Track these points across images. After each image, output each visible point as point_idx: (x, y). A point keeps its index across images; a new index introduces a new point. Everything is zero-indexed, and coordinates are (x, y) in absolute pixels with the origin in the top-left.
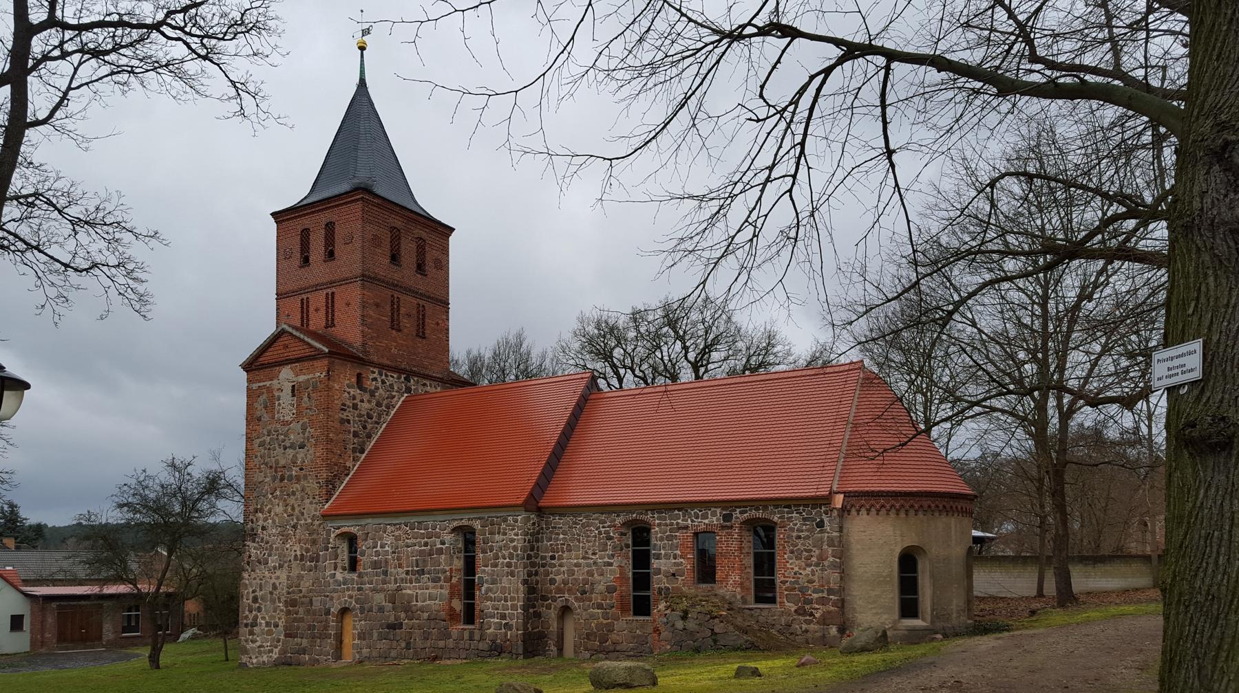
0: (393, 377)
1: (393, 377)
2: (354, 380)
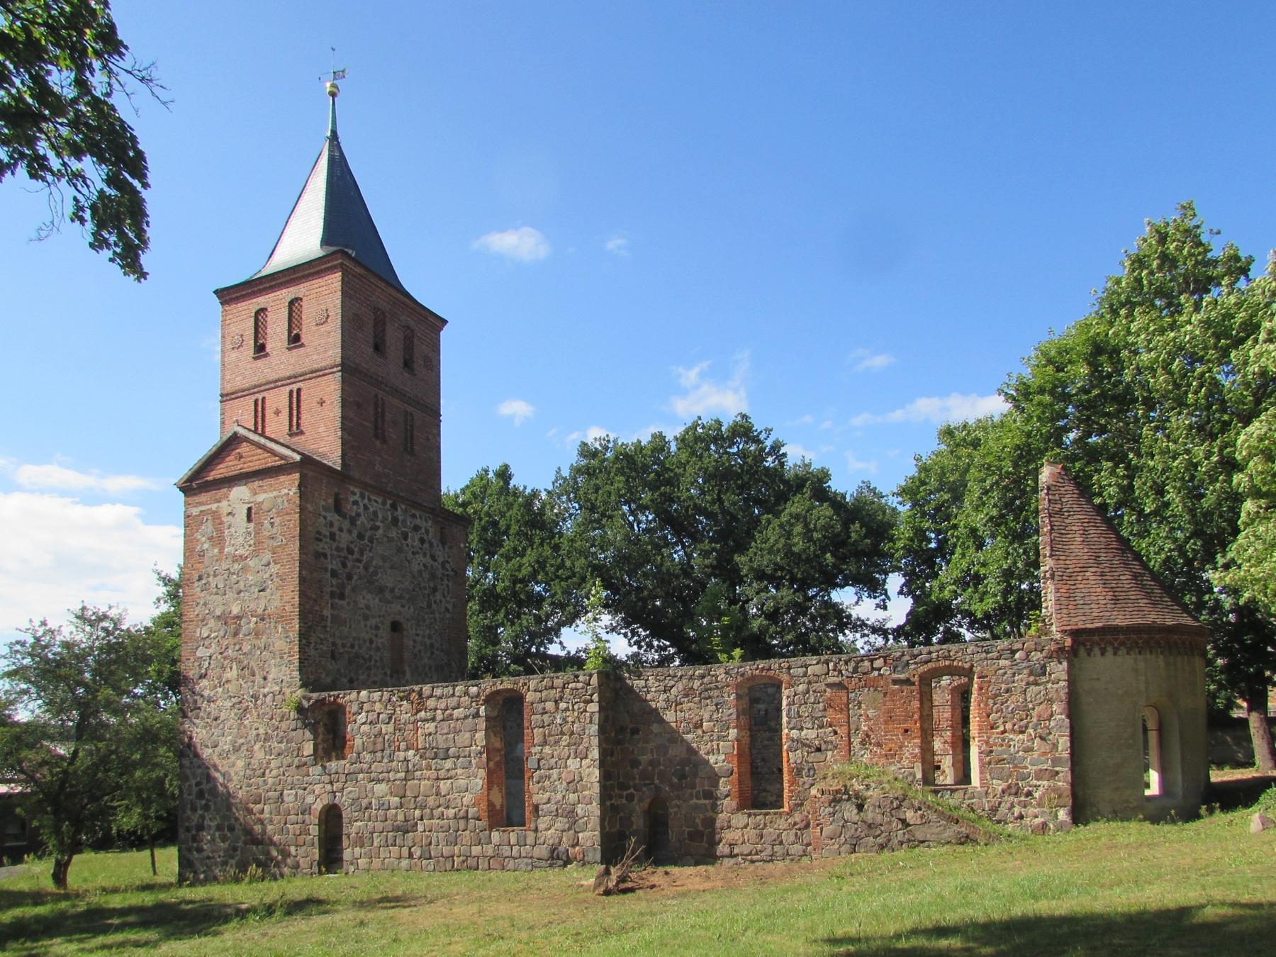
0: (376, 501)
1: (376, 501)
2: (331, 501)
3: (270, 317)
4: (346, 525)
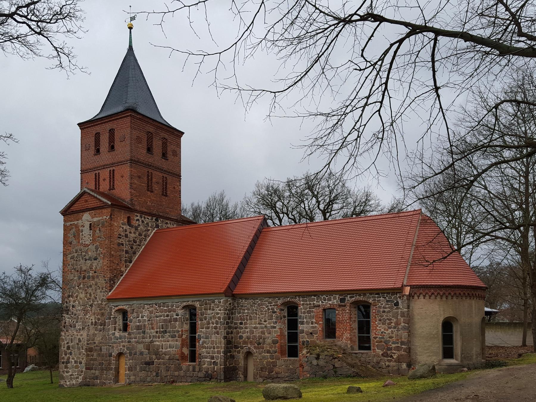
2: (126, 220)
3: (101, 138)
4: (133, 230)
